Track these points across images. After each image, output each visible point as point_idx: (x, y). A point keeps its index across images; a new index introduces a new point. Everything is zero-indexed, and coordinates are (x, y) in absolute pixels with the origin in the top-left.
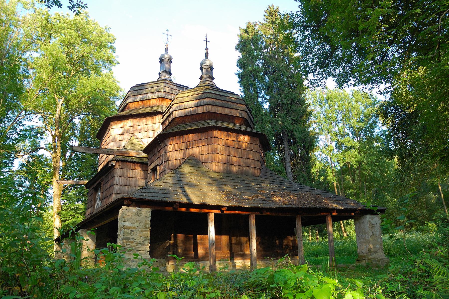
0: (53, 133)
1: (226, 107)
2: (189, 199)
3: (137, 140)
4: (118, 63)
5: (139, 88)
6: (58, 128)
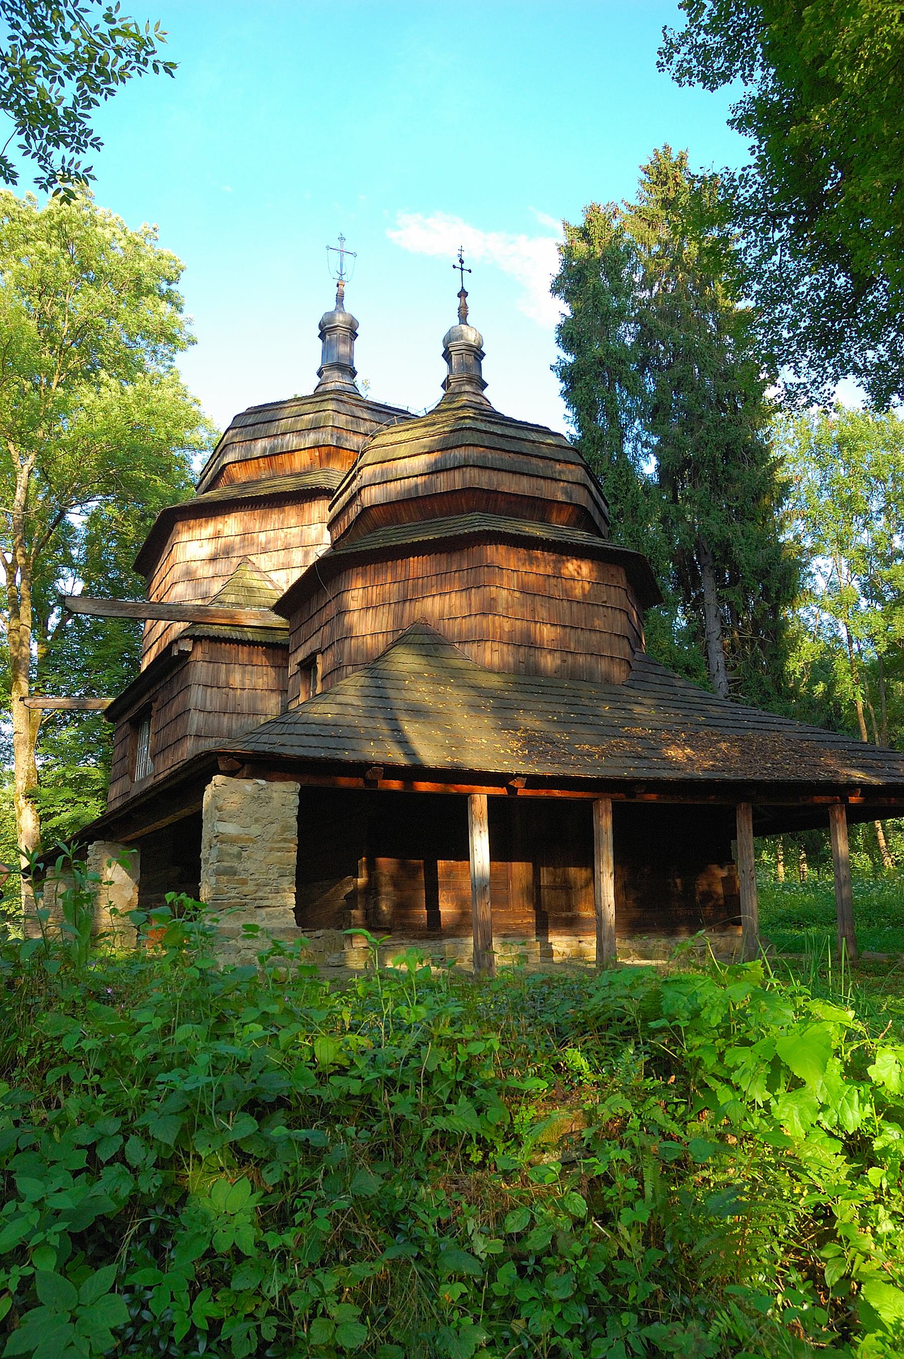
1: (523, 474)
3: (256, 576)
5: (257, 420)
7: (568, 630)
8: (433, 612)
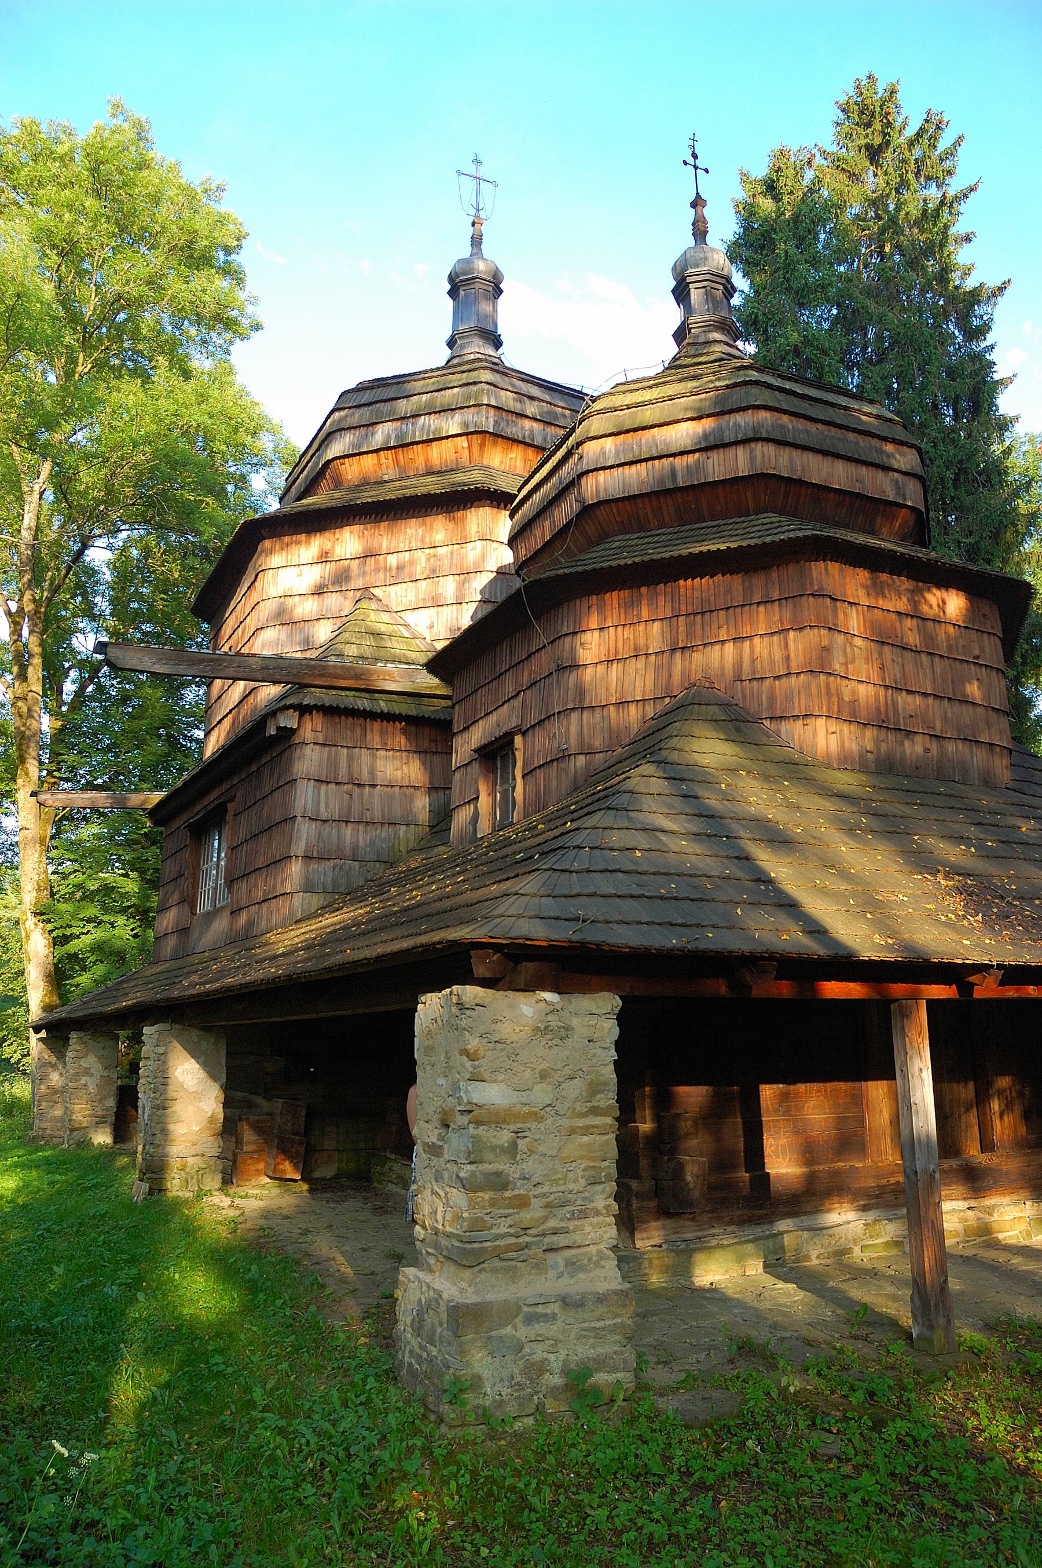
0: (13, 606)
1: (838, 456)
2: (817, 930)
3: (385, 617)
4: (257, 327)
5: (373, 399)
6: (29, 585)
7: (931, 700)
8: (722, 668)
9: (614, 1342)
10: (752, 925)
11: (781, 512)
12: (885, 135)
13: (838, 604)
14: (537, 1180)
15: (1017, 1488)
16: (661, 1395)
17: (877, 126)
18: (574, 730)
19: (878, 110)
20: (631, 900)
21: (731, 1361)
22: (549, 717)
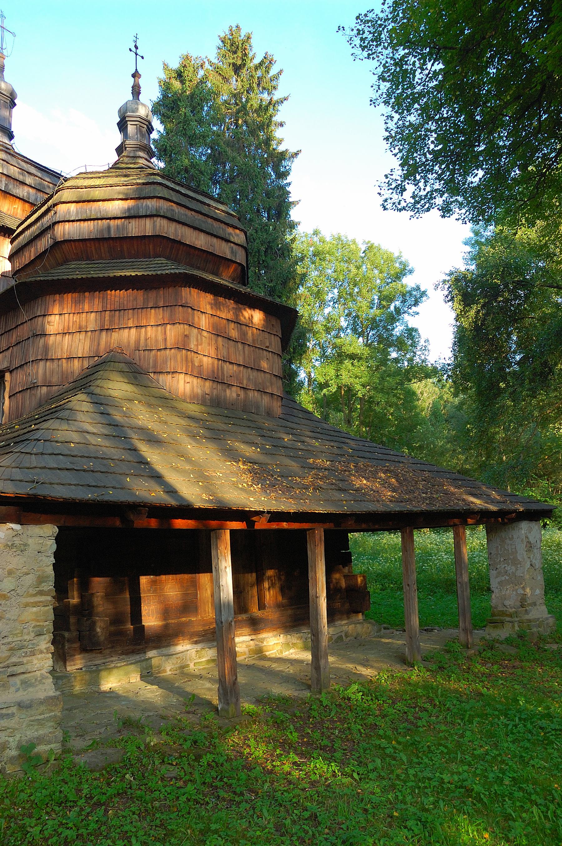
2: (171, 491)
7: (242, 368)
8: (129, 343)
9: (50, 727)
10: (135, 487)
11: (168, 258)
12: (243, 60)
13: (195, 312)
14: (5, 635)
15: (266, 781)
16: (78, 755)
17: (240, 54)
18: (41, 371)
19: (240, 45)
20: (66, 471)
21: (119, 731)
22: (26, 363)
